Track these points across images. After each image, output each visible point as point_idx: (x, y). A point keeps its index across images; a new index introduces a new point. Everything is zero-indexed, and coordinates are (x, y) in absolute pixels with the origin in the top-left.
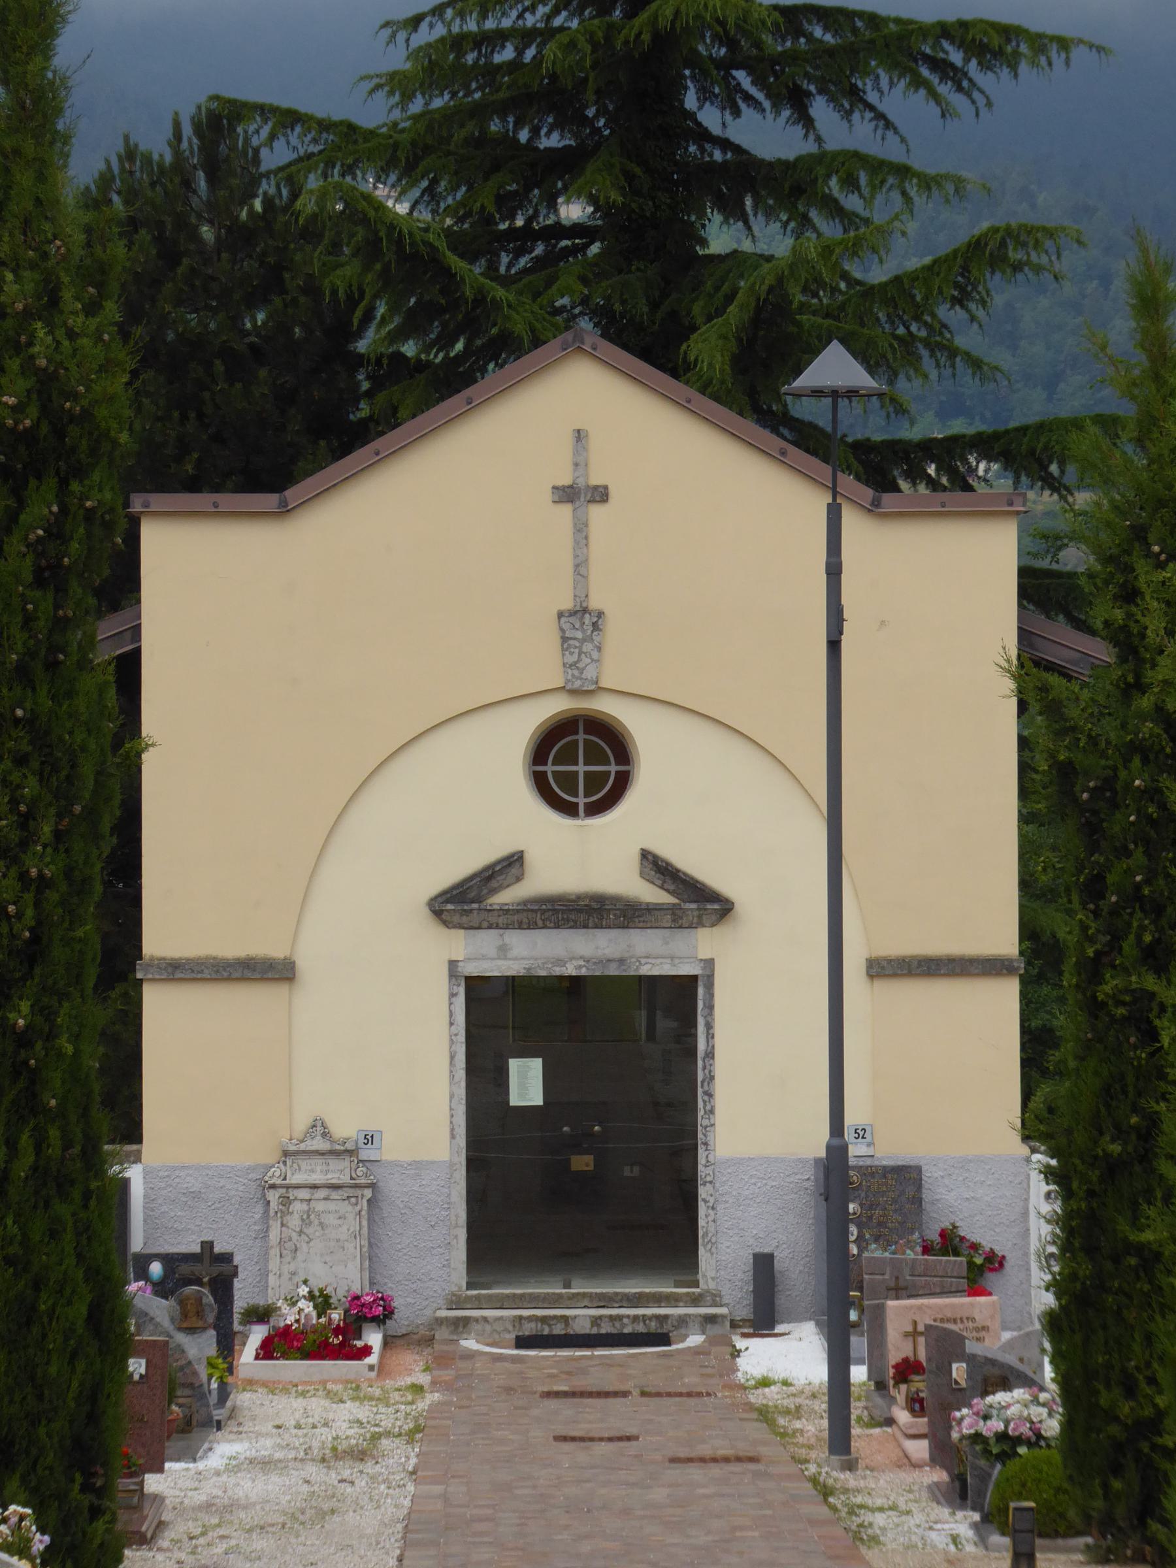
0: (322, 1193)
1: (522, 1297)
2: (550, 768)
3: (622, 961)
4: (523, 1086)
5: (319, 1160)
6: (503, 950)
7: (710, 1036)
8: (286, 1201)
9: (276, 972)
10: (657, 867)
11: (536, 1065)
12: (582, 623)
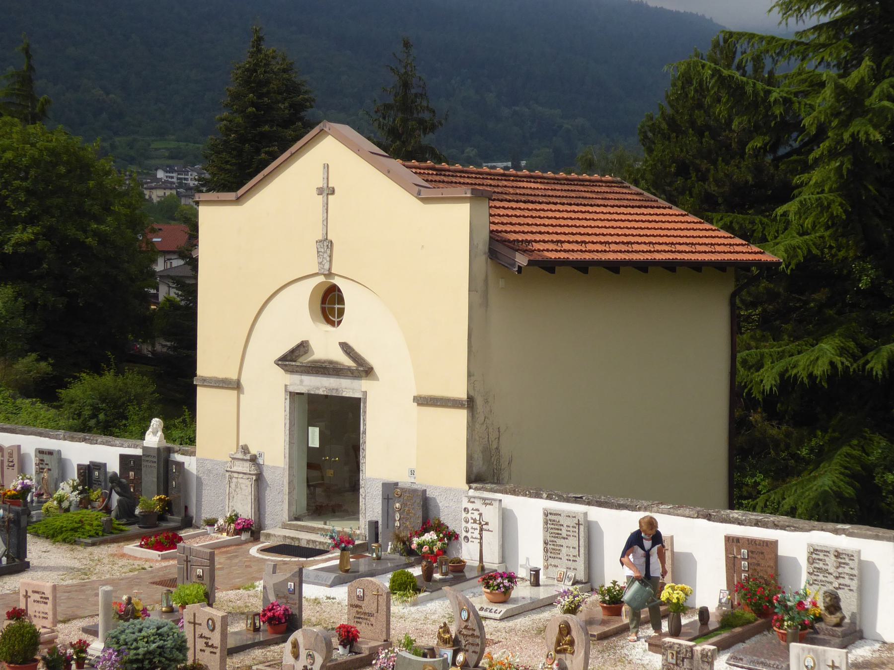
0: (241, 476)
1: (303, 526)
2: (327, 306)
3: (337, 390)
4: (313, 442)
5: (241, 462)
6: (301, 381)
7: (365, 425)
8: (231, 478)
9: (424, 401)
10: (346, 348)
11: (317, 430)
12: (326, 245)
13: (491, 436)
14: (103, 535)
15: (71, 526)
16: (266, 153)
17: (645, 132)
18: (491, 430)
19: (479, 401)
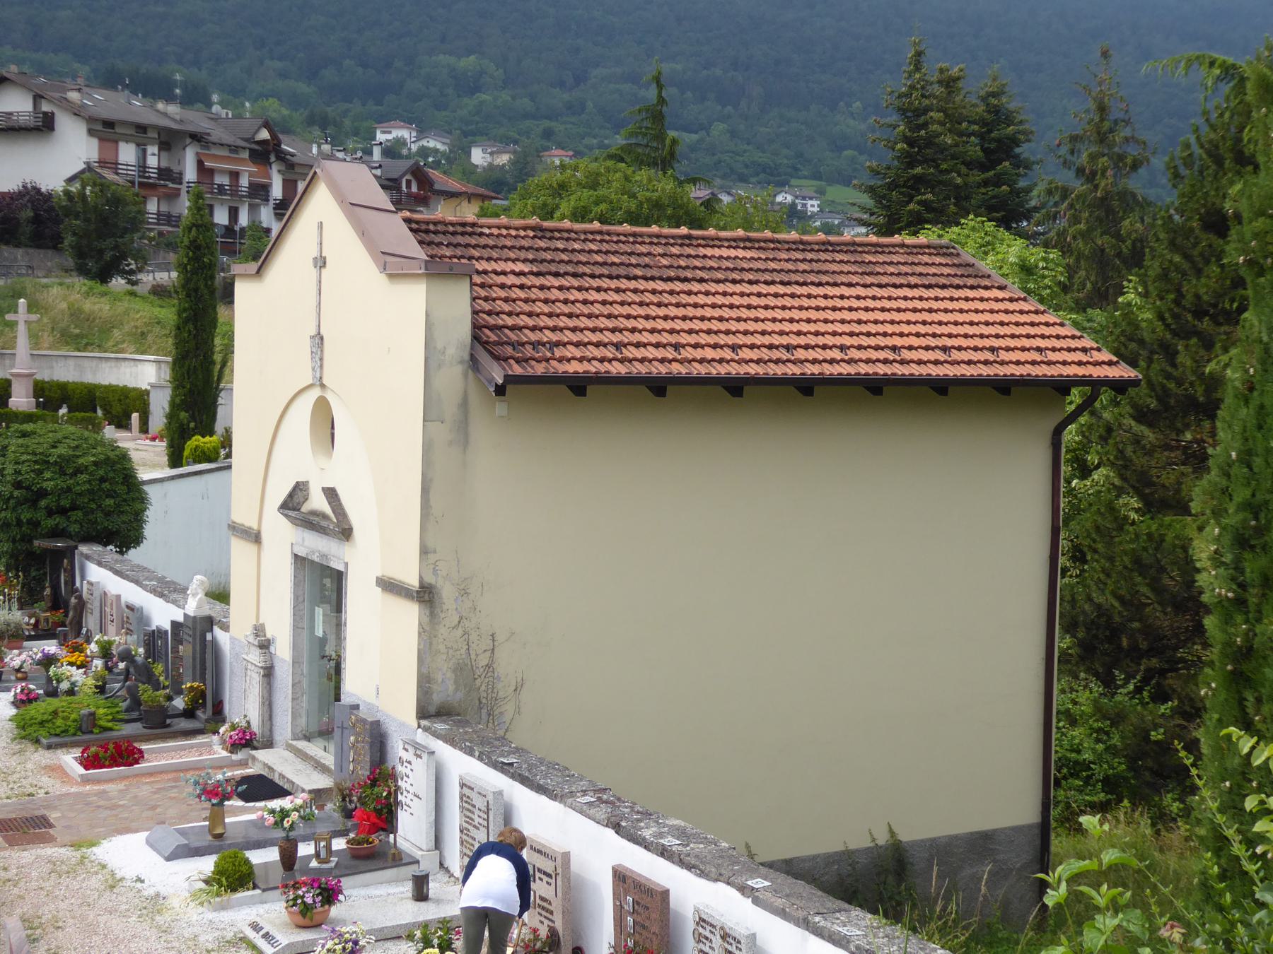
13: (473, 646)
14: (74, 735)
15: (40, 718)
16: (919, 203)
17: (1175, 167)
18: (473, 637)
19: (447, 593)
